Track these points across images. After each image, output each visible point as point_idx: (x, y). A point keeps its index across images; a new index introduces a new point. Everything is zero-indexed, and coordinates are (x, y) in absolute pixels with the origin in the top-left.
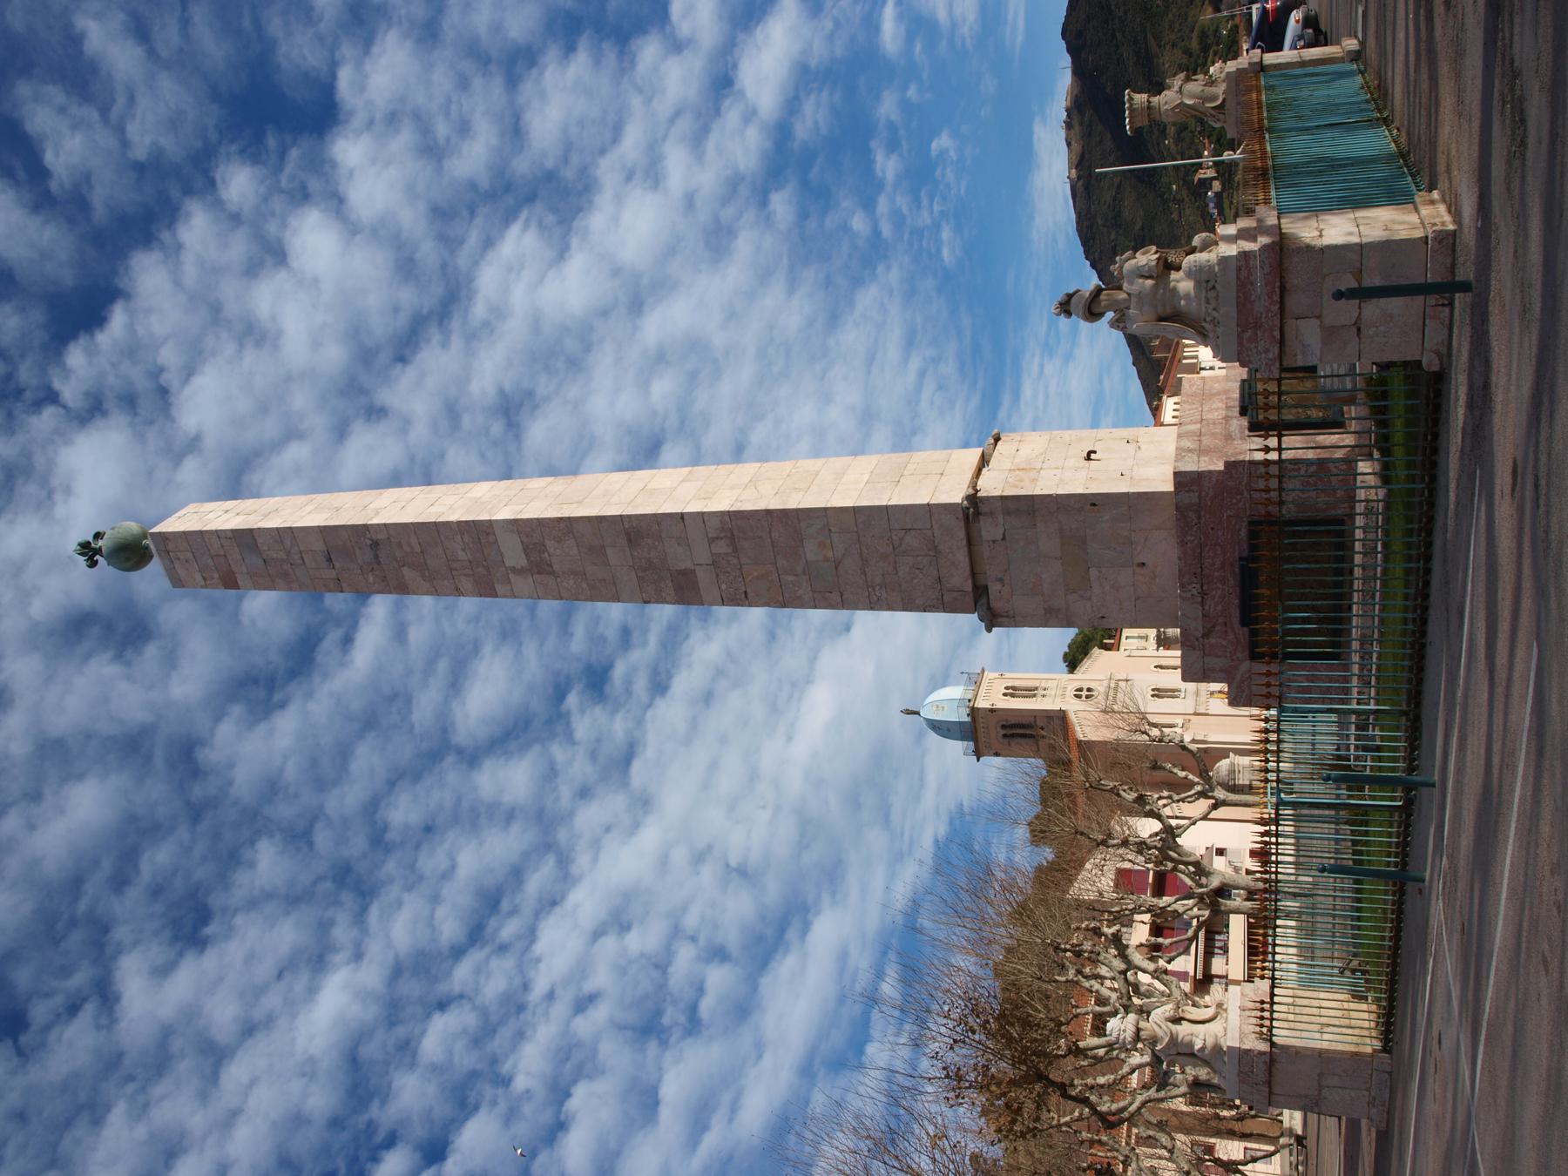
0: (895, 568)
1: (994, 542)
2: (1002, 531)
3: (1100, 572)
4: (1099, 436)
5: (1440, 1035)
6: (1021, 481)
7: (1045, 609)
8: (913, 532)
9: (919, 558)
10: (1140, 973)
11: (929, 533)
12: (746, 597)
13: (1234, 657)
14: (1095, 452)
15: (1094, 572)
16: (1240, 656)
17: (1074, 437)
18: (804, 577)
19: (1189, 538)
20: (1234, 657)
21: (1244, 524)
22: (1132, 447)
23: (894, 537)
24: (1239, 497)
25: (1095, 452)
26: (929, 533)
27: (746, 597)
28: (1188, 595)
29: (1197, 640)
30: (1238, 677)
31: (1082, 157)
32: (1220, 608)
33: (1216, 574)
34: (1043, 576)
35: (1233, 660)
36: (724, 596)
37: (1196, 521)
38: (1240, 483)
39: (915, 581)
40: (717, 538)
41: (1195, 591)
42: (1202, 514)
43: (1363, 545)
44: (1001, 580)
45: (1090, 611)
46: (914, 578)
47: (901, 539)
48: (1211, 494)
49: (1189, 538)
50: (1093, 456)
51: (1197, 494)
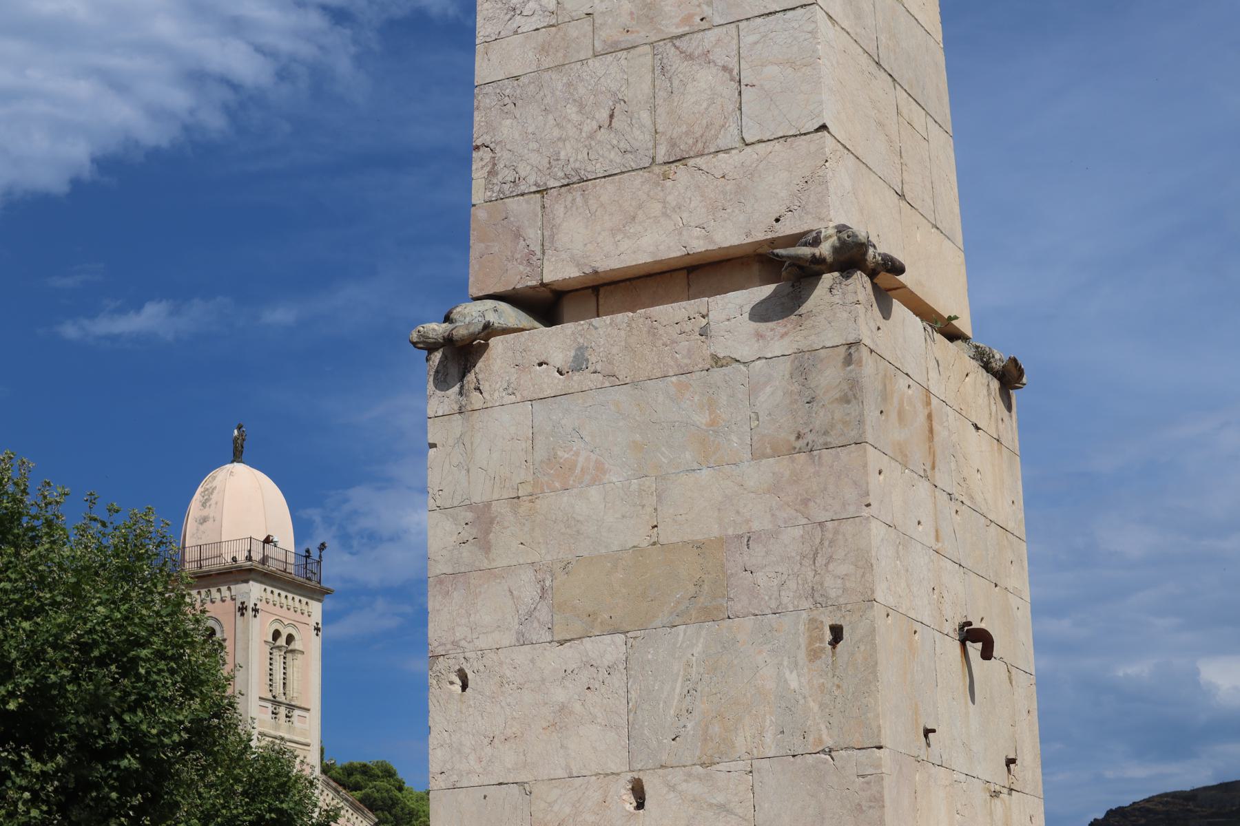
0: (614, 49)
1: (704, 332)
2: (744, 353)
4: (1020, 678)
5: (1011, 683)
6: (901, 415)
7: (488, 505)
8: (730, 89)
9: (645, 116)
11: (729, 137)
14: (987, 654)
15: (609, 648)
17: (1013, 601)
22: (999, 776)
23: (711, 36)
25: (987, 654)
26: (729, 137)
31: (1149, 810)
34: (594, 493)
39: (571, 111)
44: (579, 364)
45: (482, 643)
46: (581, 107)
47: (706, 58)
50: (975, 649)
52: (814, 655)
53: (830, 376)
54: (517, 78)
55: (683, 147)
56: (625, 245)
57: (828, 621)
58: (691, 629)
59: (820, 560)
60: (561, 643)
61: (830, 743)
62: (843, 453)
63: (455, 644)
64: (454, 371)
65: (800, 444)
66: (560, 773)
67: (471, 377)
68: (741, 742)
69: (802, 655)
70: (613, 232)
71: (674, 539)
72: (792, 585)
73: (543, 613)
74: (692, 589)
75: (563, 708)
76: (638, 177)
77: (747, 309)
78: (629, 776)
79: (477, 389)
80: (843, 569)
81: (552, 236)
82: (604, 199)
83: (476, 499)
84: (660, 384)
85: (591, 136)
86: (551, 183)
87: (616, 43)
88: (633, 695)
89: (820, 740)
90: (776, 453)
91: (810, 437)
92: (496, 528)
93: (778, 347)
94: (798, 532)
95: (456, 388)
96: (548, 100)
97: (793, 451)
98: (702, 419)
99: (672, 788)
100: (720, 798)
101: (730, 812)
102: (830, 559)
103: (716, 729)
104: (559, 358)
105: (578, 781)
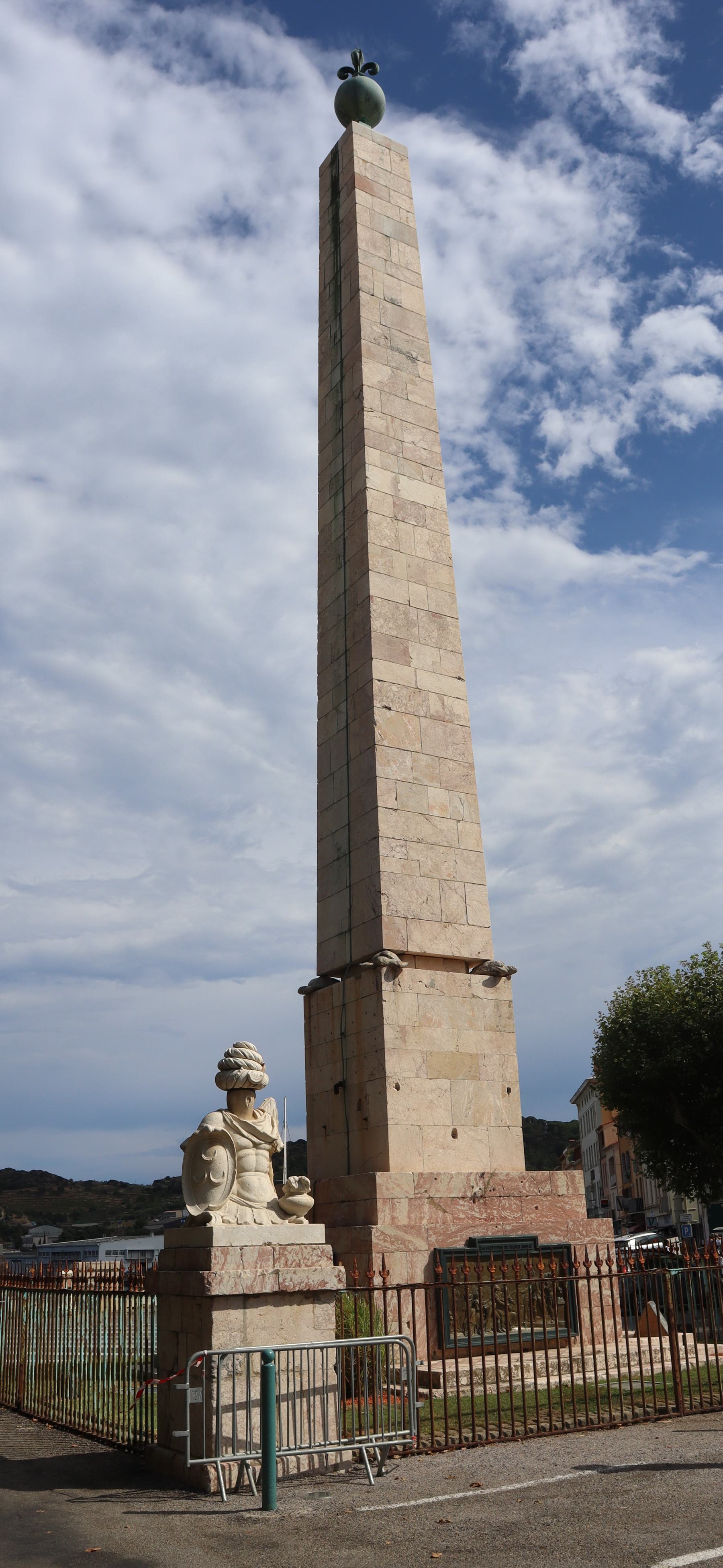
0: (426, 876)
3: (445, 1091)
7: (404, 1027)
9: (438, 904)
10: (607, 1144)
12: (386, 707)
13: (431, 1232)
15: (445, 1084)
16: (433, 1239)
18: (411, 777)
19: (527, 1184)
20: (431, 1232)
21: (562, 1238)
24: (584, 1233)
26: (463, 921)
27: (386, 707)
28: (473, 1183)
29: (426, 1191)
30: (408, 1237)
32: (462, 1216)
33: (495, 1212)
34: (438, 1030)
35: (427, 1230)
36: (386, 684)
37: (543, 1191)
38: (596, 1234)
39: (414, 892)
40: (443, 704)
41: (476, 1189)
42: (550, 1198)
43: (562, 1347)
44: (432, 985)
45: (404, 1075)
46: (417, 893)
48: (567, 1207)
49: (527, 1184)
51: (566, 1194)
52: (504, 1096)
53: (505, 1009)
54: (395, 874)
55: (450, 919)
56: (434, 946)
57: (507, 1087)
58: (469, 1081)
59: (504, 1067)
60: (430, 1079)
61: (508, 1124)
62: (509, 1034)
63: (395, 1073)
64: (391, 976)
65: (497, 1029)
66: (432, 1124)
67: (396, 980)
68: (485, 1121)
69: (500, 1096)
70: (430, 940)
71: (463, 1051)
72: (497, 1073)
73: (424, 1068)
74: (469, 1069)
75: (431, 1102)
76: (437, 925)
77: (482, 981)
78: (453, 1127)
79: (399, 984)
80: (510, 1071)
81: (410, 936)
82: (426, 928)
83: (400, 1023)
84: (457, 999)
85: (421, 904)
86: (409, 916)
87: (427, 874)
88: (453, 1101)
89: (506, 1123)
90: (491, 1030)
91: (500, 1027)
92: (407, 1035)
93: (490, 996)
94: (498, 1057)
95: (392, 982)
96: (406, 886)
97: (495, 1030)
98: (470, 1014)
99: (466, 1133)
100: (479, 1138)
101: (482, 1142)
102: (507, 1067)
103: (477, 1115)
104: (426, 981)
105: (437, 1127)
